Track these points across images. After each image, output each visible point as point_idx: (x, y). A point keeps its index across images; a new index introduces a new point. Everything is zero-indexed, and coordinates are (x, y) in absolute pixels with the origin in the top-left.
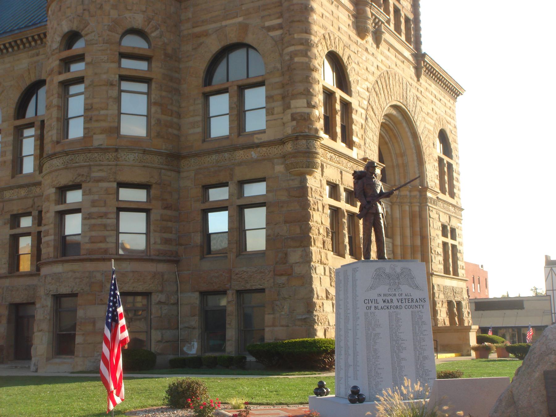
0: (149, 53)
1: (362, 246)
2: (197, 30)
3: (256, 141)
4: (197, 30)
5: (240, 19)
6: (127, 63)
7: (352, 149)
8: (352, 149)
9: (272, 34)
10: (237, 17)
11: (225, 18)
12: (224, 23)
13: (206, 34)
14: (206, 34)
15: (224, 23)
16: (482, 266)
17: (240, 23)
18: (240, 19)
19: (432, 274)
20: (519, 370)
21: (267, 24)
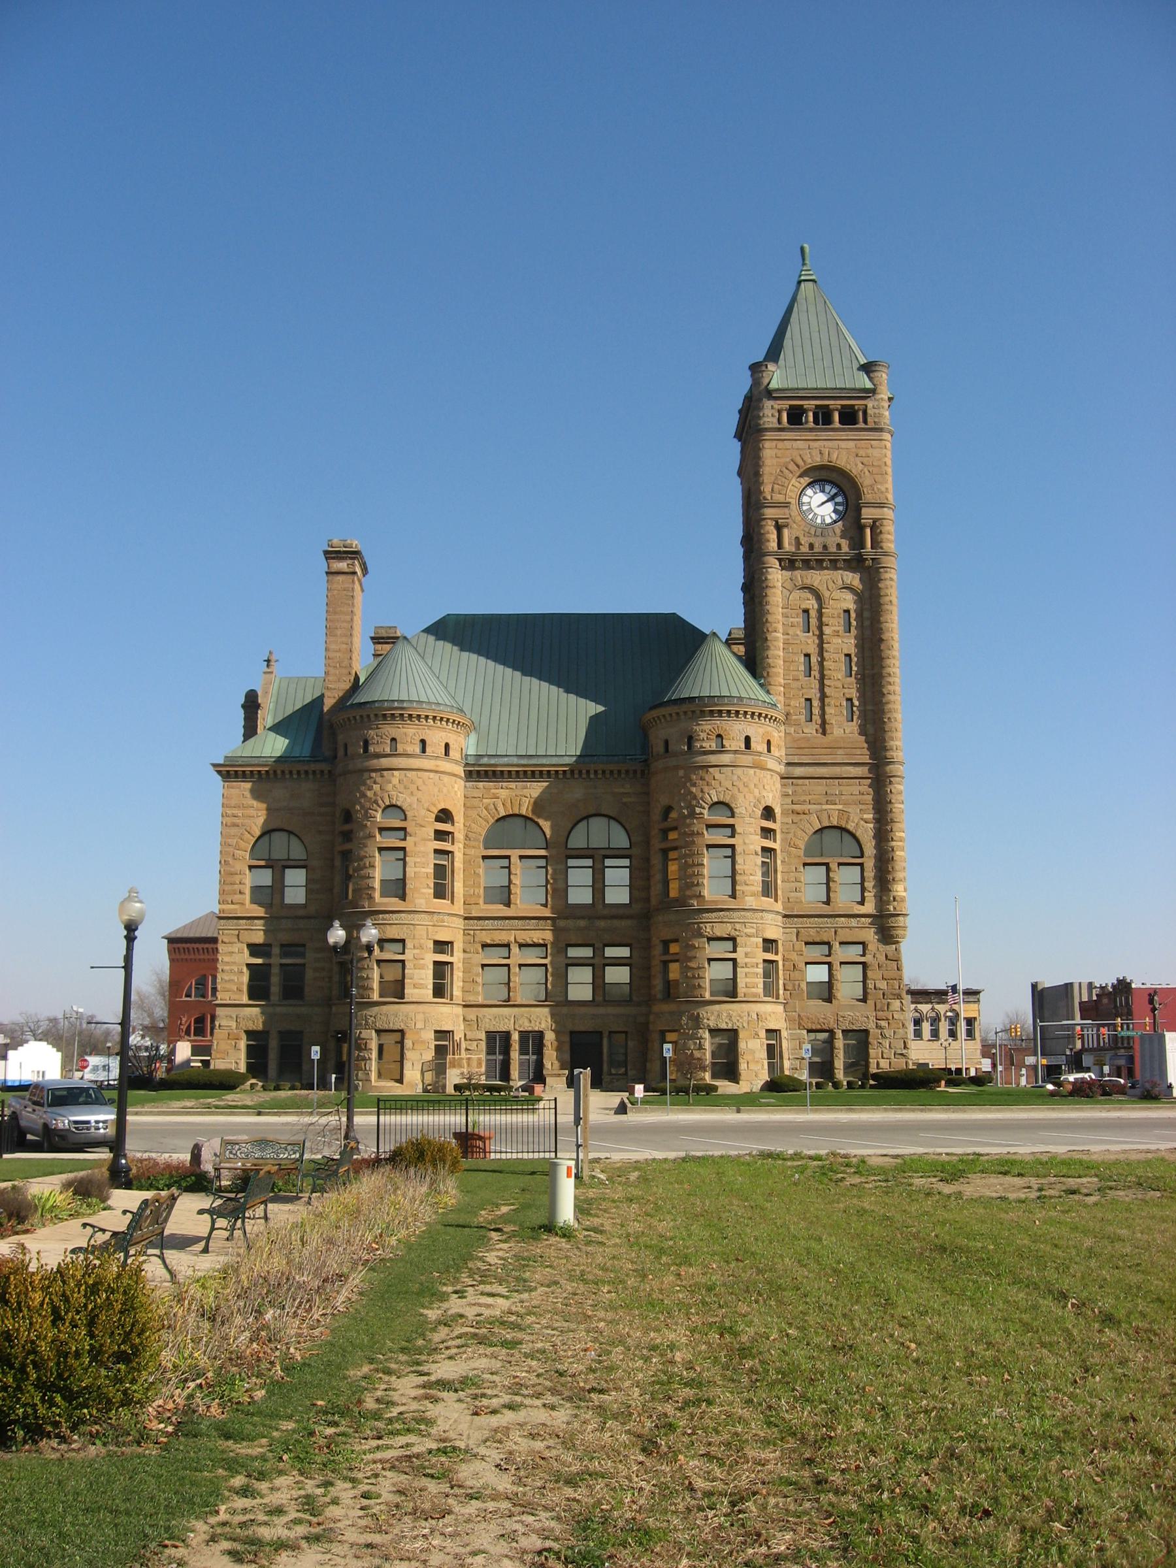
2: (796, 807)
4: (796, 807)
12: (824, 807)
18: (840, 807)
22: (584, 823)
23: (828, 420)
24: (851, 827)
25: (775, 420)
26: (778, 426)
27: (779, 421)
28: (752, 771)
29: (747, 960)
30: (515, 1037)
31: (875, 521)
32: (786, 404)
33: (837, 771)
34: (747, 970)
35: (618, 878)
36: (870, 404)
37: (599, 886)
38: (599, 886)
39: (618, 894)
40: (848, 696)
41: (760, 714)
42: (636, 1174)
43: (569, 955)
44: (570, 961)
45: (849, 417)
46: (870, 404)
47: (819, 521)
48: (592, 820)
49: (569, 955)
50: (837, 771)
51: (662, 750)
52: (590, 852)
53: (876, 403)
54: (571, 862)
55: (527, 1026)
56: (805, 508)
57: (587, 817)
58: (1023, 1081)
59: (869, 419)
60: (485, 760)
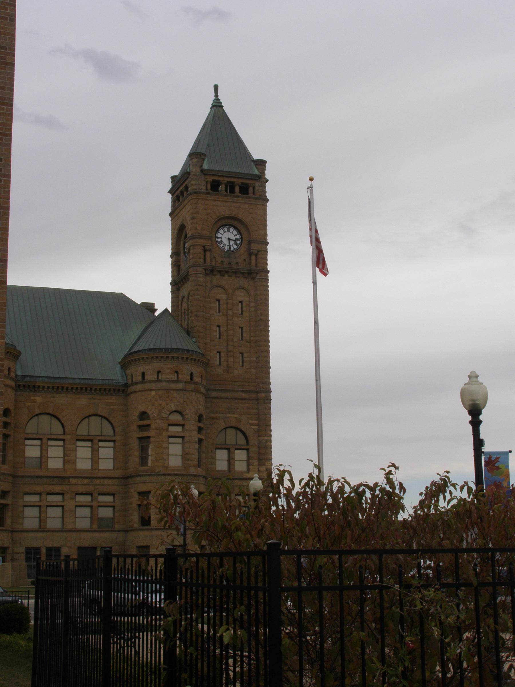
0: (182, 423)
1: (270, 542)
2: (212, 415)
3: (245, 477)
4: (212, 415)
5: (236, 416)
6: (171, 428)
7: (157, 309)
8: (157, 309)
9: (253, 427)
10: (234, 414)
11: (230, 413)
12: (228, 415)
13: (218, 419)
14: (218, 419)
15: (228, 415)
16: (421, 494)
17: (236, 417)
18: (236, 416)
19: (48, 457)
20: (150, 307)
21: (250, 421)
22: (87, 420)
23: (232, 191)
24: (242, 427)
25: (204, 188)
26: (205, 191)
27: (206, 189)
30: (44, 551)
31: (258, 251)
32: (210, 179)
33: (235, 395)
35: (106, 452)
36: (257, 184)
37: (95, 459)
38: (95, 459)
39: (106, 464)
40: (241, 351)
41: (199, 360)
42: (471, 559)
43: (48, 500)
44: (48, 504)
45: (244, 190)
46: (257, 184)
47: (222, 246)
48: (40, 416)
49: (48, 500)
50: (235, 395)
51: (140, 378)
52: (91, 438)
53: (260, 184)
54: (79, 443)
55: (50, 544)
56: (219, 240)
57: (88, 417)
58: (490, 545)
59: (256, 192)
60: (28, 379)
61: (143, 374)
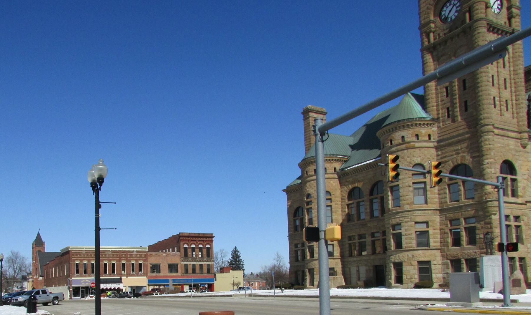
18: (461, 155)
28: (406, 151)
29: (406, 232)
34: (406, 236)
61: (403, 137)
